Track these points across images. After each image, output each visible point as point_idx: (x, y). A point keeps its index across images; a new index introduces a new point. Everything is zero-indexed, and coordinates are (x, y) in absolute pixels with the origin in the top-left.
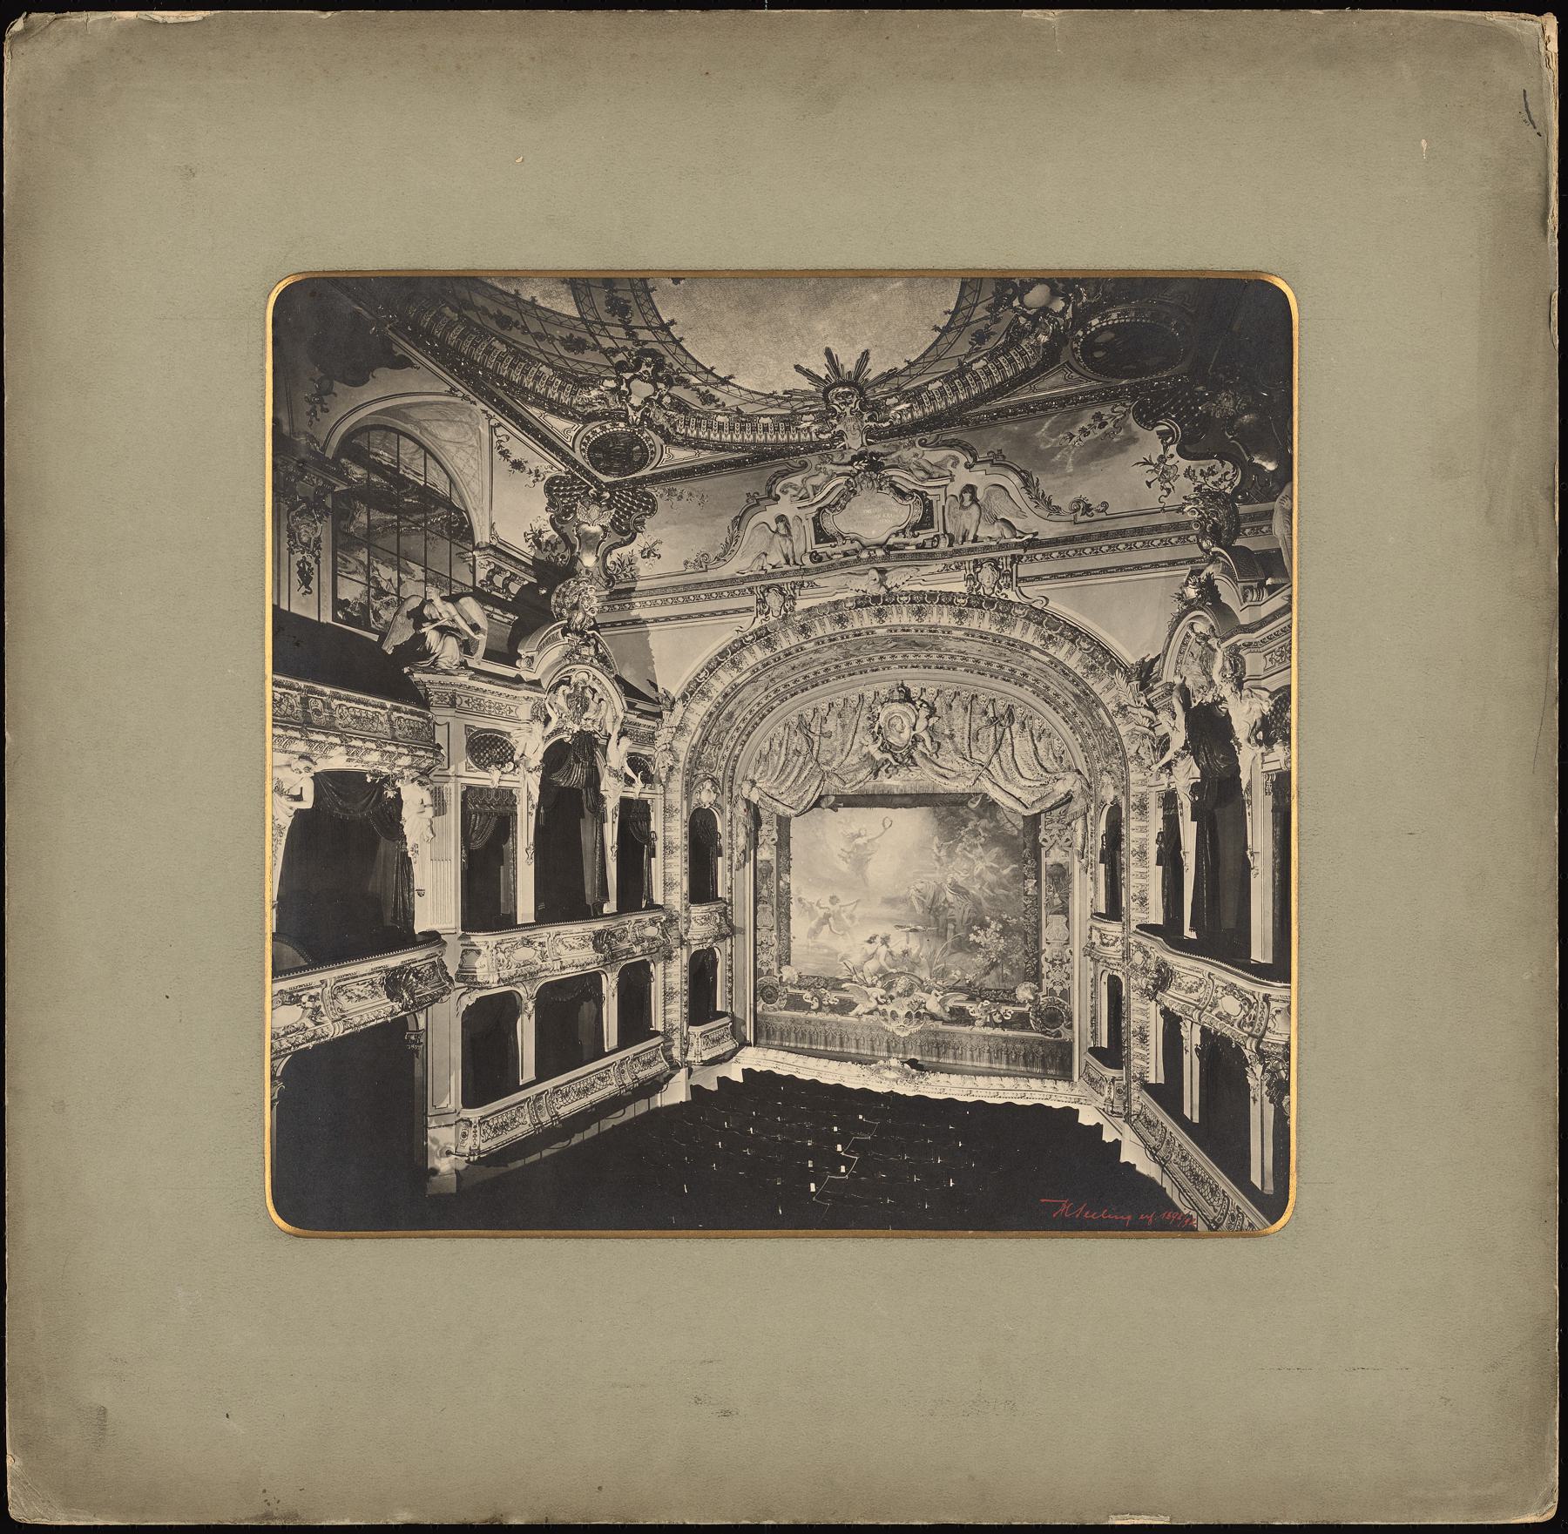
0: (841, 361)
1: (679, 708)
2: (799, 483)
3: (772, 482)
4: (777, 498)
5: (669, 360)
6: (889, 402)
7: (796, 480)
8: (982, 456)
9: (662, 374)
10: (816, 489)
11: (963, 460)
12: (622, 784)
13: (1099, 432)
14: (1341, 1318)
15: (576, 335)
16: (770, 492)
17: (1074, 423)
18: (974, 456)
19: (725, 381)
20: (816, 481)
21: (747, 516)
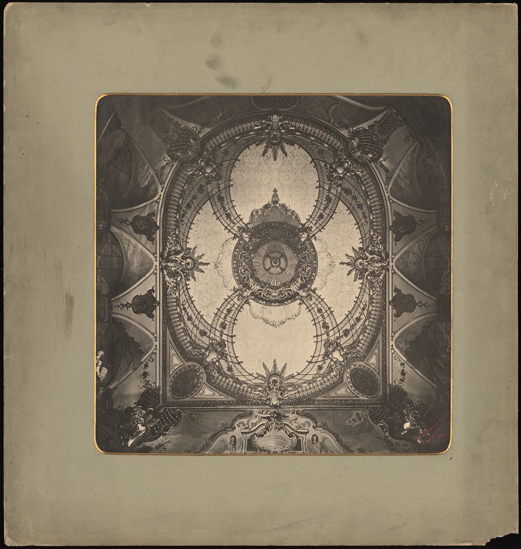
0: (277, 366)
1: (350, 332)
2: (246, 423)
3: (235, 420)
4: (235, 428)
5: (226, 349)
6: (289, 389)
7: (245, 420)
8: (319, 424)
9: (223, 355)
10: (254, 425)
11: (312, 424)
12: (282, 430)
13: (360, 422)
14: (73, 70)
15: (206, 330)
16: (232, 424)
17: (350, 416)
18: (316, 423)
19: (239, 363)
20: (254, 421)
21: (217, 435)
